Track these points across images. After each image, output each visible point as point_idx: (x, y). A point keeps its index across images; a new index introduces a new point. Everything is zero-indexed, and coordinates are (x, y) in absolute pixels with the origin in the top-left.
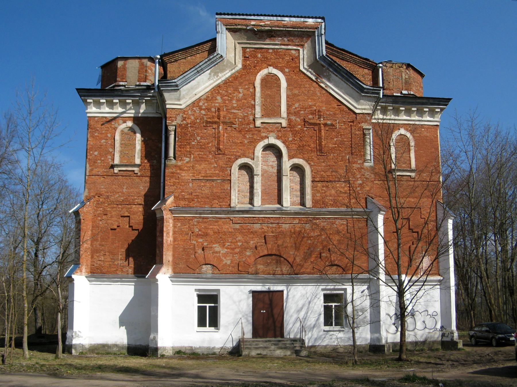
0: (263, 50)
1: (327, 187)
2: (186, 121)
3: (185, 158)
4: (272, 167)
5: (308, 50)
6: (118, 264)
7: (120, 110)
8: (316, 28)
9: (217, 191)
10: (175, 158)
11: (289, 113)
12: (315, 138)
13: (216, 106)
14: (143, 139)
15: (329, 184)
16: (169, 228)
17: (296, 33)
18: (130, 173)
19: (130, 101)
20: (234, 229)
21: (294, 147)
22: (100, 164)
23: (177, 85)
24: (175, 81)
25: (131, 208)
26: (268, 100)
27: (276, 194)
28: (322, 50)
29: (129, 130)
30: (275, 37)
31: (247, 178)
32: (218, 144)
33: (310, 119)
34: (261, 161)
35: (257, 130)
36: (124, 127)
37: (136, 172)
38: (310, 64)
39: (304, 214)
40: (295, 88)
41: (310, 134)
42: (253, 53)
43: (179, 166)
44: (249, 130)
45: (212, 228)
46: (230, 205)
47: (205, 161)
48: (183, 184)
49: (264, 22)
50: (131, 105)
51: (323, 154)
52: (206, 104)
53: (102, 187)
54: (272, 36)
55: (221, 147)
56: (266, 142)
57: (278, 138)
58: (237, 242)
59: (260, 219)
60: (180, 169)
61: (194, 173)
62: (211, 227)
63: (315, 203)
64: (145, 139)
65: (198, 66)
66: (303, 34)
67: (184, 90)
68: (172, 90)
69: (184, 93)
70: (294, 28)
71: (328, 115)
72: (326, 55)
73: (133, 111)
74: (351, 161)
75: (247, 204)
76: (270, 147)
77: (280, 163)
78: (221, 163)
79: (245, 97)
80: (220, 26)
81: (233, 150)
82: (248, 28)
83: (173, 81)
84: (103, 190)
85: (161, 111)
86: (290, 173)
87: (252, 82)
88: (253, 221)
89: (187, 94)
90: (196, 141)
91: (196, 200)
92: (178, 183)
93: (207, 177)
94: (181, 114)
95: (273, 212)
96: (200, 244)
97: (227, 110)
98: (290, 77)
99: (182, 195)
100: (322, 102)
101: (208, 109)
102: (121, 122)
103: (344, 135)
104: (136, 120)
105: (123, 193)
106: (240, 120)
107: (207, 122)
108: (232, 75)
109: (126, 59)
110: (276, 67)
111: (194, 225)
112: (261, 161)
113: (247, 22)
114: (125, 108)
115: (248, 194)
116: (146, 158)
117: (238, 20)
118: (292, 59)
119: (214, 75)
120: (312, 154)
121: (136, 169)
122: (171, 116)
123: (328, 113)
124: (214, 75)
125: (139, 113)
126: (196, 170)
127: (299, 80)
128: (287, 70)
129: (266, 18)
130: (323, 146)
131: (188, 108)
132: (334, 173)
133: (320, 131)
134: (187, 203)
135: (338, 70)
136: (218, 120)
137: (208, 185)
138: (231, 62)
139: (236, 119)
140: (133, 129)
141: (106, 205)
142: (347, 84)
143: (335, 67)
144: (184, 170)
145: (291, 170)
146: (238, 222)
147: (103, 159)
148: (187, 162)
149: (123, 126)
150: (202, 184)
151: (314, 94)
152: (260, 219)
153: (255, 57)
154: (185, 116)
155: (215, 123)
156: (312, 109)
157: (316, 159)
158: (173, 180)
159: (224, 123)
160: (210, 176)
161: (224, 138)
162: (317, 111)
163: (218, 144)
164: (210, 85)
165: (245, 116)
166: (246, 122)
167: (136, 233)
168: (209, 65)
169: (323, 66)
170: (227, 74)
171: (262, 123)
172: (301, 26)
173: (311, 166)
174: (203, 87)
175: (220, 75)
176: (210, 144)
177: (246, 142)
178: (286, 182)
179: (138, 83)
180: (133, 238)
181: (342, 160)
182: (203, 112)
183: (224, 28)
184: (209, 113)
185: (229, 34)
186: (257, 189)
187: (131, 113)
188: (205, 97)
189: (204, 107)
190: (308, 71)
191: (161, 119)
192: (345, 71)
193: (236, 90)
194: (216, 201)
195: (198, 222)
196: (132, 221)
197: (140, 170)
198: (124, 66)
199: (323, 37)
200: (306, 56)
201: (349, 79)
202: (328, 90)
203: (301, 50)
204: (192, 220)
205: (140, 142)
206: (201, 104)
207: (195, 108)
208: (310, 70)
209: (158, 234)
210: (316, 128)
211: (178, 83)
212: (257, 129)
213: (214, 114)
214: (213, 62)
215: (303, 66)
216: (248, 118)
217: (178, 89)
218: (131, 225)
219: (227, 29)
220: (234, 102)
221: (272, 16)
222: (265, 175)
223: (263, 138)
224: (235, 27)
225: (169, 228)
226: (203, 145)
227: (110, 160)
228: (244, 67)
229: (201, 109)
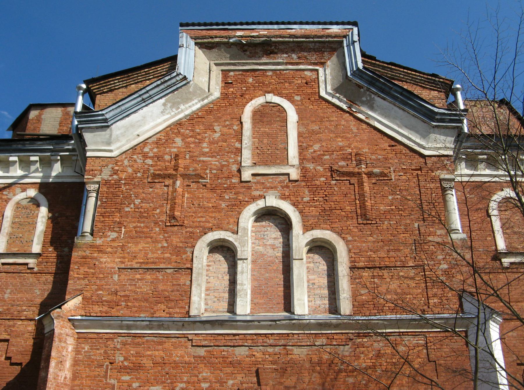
0: (258, 73)
1: (381, 277)
2: (118, 175)
4: (273, 247)
5: (331, 70)
7: (20, 173)
8: (345, 37)
9: (164, 288)
11: (302, 158)
12: (353, 197)
13: (174, 152)
14: (50, 215)
15: (385, 273)
17: (311, 46)
19: (37, 158)
20: (194, 357)
21: (314, 211)
23: (106, 119)
24: (104, 112)
25: (14, 327)
26: (265, 141)
27: (282, 294)
29: (29, 202)
30: (276, 53)
32: (172, 209)
33: (342, 167)
34: (250, 237)
36: (22, 198)
37: (30, 266)
38: (336, 86)
39: (336, 326)
40: (313, 122)
41: (340, 188)
42: (240, 77)
43: (97, 247)
45: (150, 356)
46: (188, 312)
47: (146, 237)
48: (101, 276)
50: (38, 165)
51: (370, 222)
52: (155, 150)
54: (272, 52)
55: (177, 214)
56: (261, 204)
57: (283, 197)
58: (199, 381)
59: (248, 337)
60: (100, 251)
62: (149, 353)
63: (359, 306)
64: (53, 215)
65: (144, 91)
66: (324, 47)
67: (118, 128)
68: (97, 128)
69: (118, 132)
72: (364, 68)
73: (41, 175)
75: (224, 312)
76: (268, 214)
77: (288, 240)
78: (175, 240)
79: (224, 138)
80: (184, 39)
81: (199, 220)
82: (231, 41)
86: (308, 258)
88: (234, 341)
89: (123, 135)
91: (123, 304)
92: (93, 274)
93: (147, 263)
94: (110, 166)
95: (274, 323)
96: (126, 384)
97: (191, 157)
99: (98, 295)
100: (361, 141)
101: (159, 158)
102: (18, 190)
104: (44, 188)
106: (215, 172)
107: (155, 176)
108: (203, 107)
109: (42, 106)
111: (115, 349)
112: (250, 237)
114: (29, 171)
115: (227, 295)
116: (52, 245)
117: (215, 32)
118: (306, 83)
119: (172, 107)
121: (32, 262)
122: (94, 168)
123: (373, 157)
124: (172, 107)
125: (49, 177)
126: (128, 253)
128: (297, 98)
129: (261, 27)
132: (392, 254)
133: (361, 184)
134: (105, 309)
135: (387, 89)
136: (174, 173)
137: (149, 277)
138: (201, 89)
139: (206, 170)
140: (36, 201)
142: (404, 110)
143: (380, 85)
145: (310, 251)
146: (204, 343)
148: (113, 240)
149: (21, 196)
150: (138, 276)
152: (248, 337)
154: (117, 168)
155: (169, 176)
156: (344, 152)
157: (356, 230)
159: (184, 176)
160: (153, 263)
161: (184, 199)
163: (172, 209)
164: (165, 121)
165: (223, 166)
166: (226, 175)
167: (17, 369)
168: (163, 91)
169: (360, 87)
170: (195, 105)
171: (253, 175)
173: (347, 242)
174: (152, 124)
175: (182, 107)
176: (158, 211)
177: (223, 205)
178: (299, 271)
180: (11, 379)
181: (406, 231)
182: (149, 162)
183: (192, 42)
185: (200, 52)
186: (242, 284)
187: (37, 177)
188: (154, 139)
189: (151, 154)
190: (333, 97)
192: (400, 91)
194: (163, 307)
195: (124, 344)
199: (357, 45)
200: (329, 78)
201: (407, 101)
202: (372, 122)
205: (45, 220)
206: (146, 150)
207: (135, 157)
208: (338, 95)
210: (354, 180)
211: (107, 116)
212: (245, 184)
214: (170, 86)
217: (108, 127)
218: (8, 355)
219: (196, 44)
220: (205, 145)
221: (271, 23)
223: (254, 199)
224: (210, 40)
225: (64, 353)
226: (145, 212)
228: (225, 96)
229: (145, 156)
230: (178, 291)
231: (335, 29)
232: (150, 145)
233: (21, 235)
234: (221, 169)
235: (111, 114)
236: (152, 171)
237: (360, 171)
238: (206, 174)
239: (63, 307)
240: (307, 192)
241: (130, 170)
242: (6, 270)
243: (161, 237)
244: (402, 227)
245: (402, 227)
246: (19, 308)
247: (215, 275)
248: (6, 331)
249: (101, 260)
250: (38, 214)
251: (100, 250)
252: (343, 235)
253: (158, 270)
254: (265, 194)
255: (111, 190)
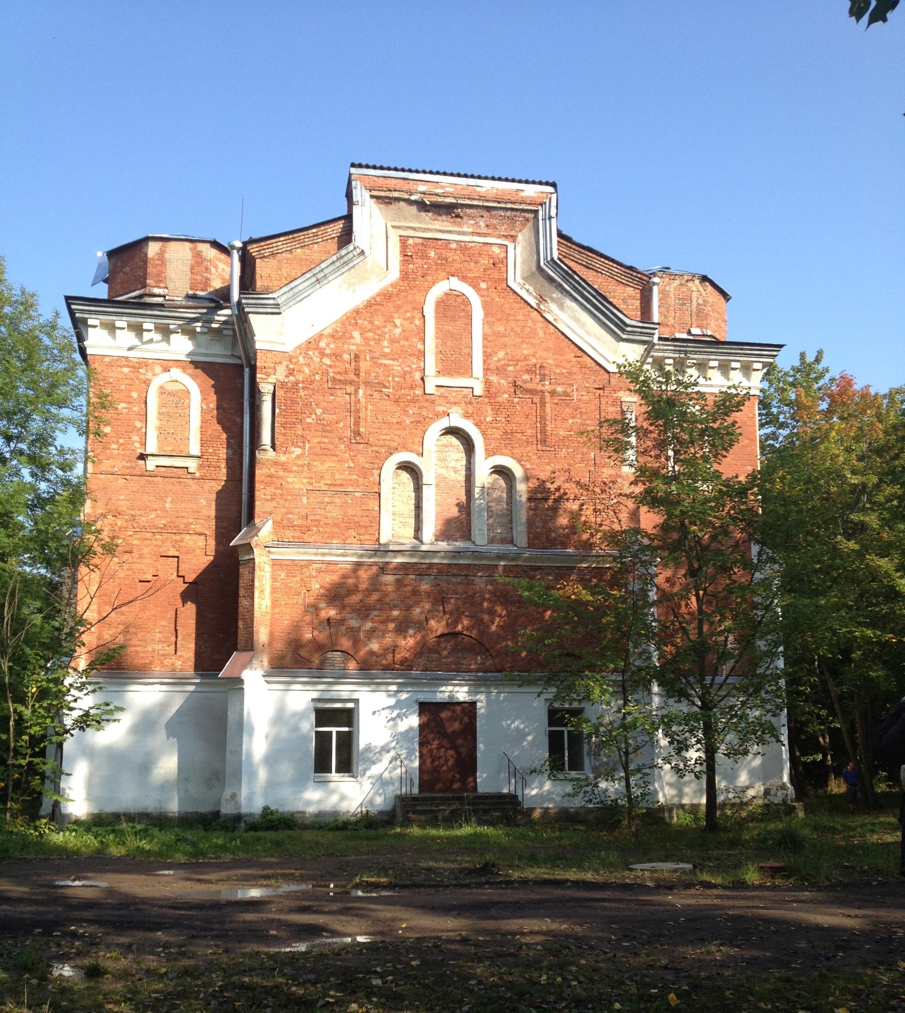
0: (440, 243)
2: (294, 376)
3: (293, 449)
5: (523, 247)
6: (154, 651)
8: (541, 205)
10: (273, 447)
11: (486, 370)
12: (534, 419)
13: (353, 351)
16: (264, 582)
18: (180, 472)
21: (497, 434)
22: (116, 452)
25: (182, 541)
28: (551, 249)
31: (411, 486)
32: (357, 424)
33: (525, 382)
35: (427, 401)
40: (499, 320)
42: (420, 247)
44: (414, 400)
49: (443, 187)
51: (548, 449)
53: (122, 497)
55: (362, 430)
56: (444, 423)
57: (467, 416)
60: (285, 470)
61: (310, 478)
65: (318, 269)
67: (288, 313)
70: (499, 202)
71: (558, 374)
74: (598, 462)
76: (452, 431)
78: (361, 460)
81: (383, 437)
83: (270, 296)
84: (123, 505)
85: (240, 351)
87: (420, 306)
90: (314, 416)
91: (315, 529)
92: (281, 495)
93: (335, 485)
94: (285, 363)
97: (372, 358)
98: (489, 299)
100: (547, 349)
101: (336, 356)
103: (586, 413)
105: (164, 510)
106: (397, 379)
110: (464, 279)
113: (411, 186)
117: (393, 181)
120: (529, 449)
121: (192, 465)
122: (267, 365)
123: (558, 371)
127: (507, 306)
128: (483, 285)
130: (549, 433)
131: (298, 352)
133: (543, 404)
134: (297, 534)
139: (388, 376)
141: (130, 533)
144: (292, 472)
147: (121, 441)
148: (298, 457)
150: (327, 499)
151: (534, 332)
153: (425, 256)
154: (292, 366)
155: (351, 383)
158: (270, 490)
159: (367, 384)
160: (341, 485)
161: (368, 412)
162: (538, 366)
163: (357, 424)
165: (405, 372)
172: (513, 199)
176: (341, 424)
177: (408, 422)
179: (191, 292)
182: (327, 361)
183: (367, 194)
184: (338, 363)
188: (329, 331)
189: (328, 351)
191: (240, 367)
193: (389, 320)
196: (182, 566)
197: (201, 467)
198: (161, 254)
199: (554, 221)
200: (519, 260)
201: (600, 306)
203: (511, 246)
204: (307, 566)
206: (322, 344)
207: (311, 353)
208: (527, 286)
209: (242, 592)
213: (348, 366)
215: (516, 280)
216: (411, 377)
218: (180, 574)
220: (385, 343)
221: (459, 175)
222: (442, 485)
223: (438, 416)
227: (137, 445)
228: (405, 275)
229: (322, 354)
230: (367, 516)
231: (531, 191)
232: (326, 337)
233: (173, 431)
234: (404, 375)
235: (283, 298)
236: (332, 374)
237: (543, 388)
238: (389, 382)
239: (259, 534)
240: (490, 411)
241: (307, 370)
242: (162, 474)
243: (347, 455)
244: (579, 456)
245: (579, 456)
246: (184, 520)
247: (400, 498)
248: (174, 546)
249: (289, 480)
250: (189, 404)
251: (284, 467)
252: (522, 463)
253: (346, 493)
254: (449, 411)
255: (289, 395)
